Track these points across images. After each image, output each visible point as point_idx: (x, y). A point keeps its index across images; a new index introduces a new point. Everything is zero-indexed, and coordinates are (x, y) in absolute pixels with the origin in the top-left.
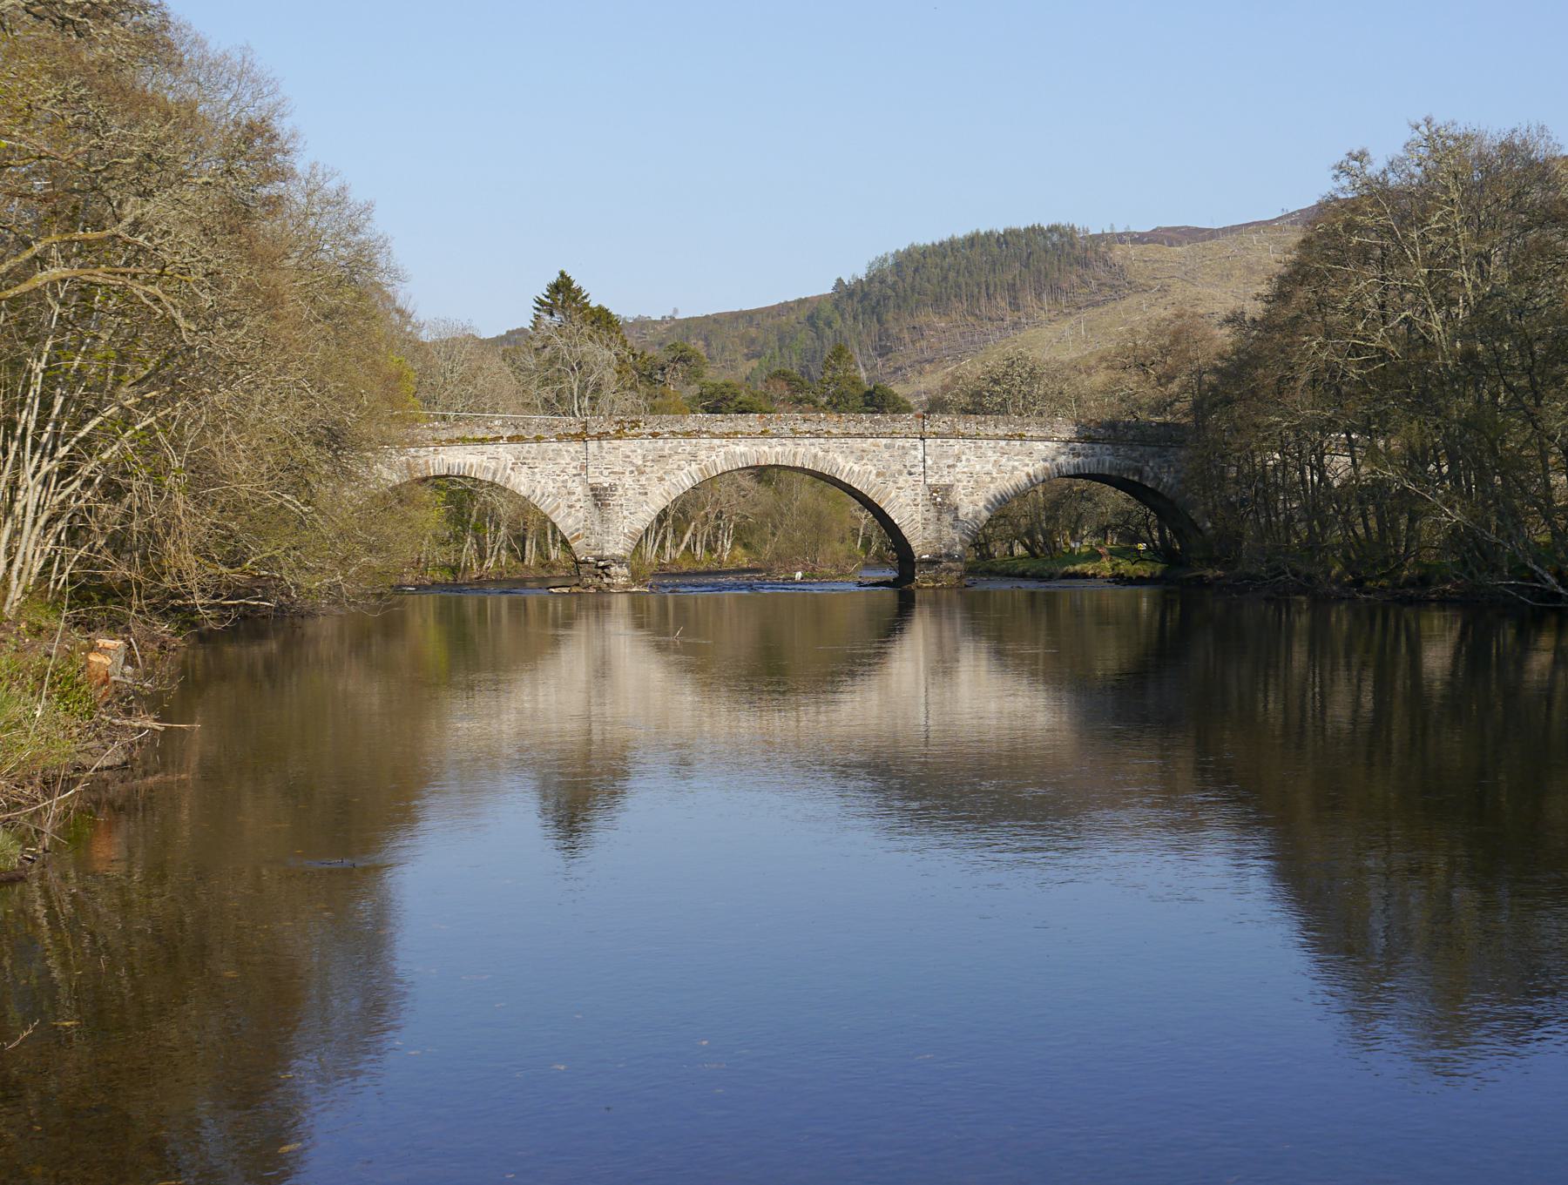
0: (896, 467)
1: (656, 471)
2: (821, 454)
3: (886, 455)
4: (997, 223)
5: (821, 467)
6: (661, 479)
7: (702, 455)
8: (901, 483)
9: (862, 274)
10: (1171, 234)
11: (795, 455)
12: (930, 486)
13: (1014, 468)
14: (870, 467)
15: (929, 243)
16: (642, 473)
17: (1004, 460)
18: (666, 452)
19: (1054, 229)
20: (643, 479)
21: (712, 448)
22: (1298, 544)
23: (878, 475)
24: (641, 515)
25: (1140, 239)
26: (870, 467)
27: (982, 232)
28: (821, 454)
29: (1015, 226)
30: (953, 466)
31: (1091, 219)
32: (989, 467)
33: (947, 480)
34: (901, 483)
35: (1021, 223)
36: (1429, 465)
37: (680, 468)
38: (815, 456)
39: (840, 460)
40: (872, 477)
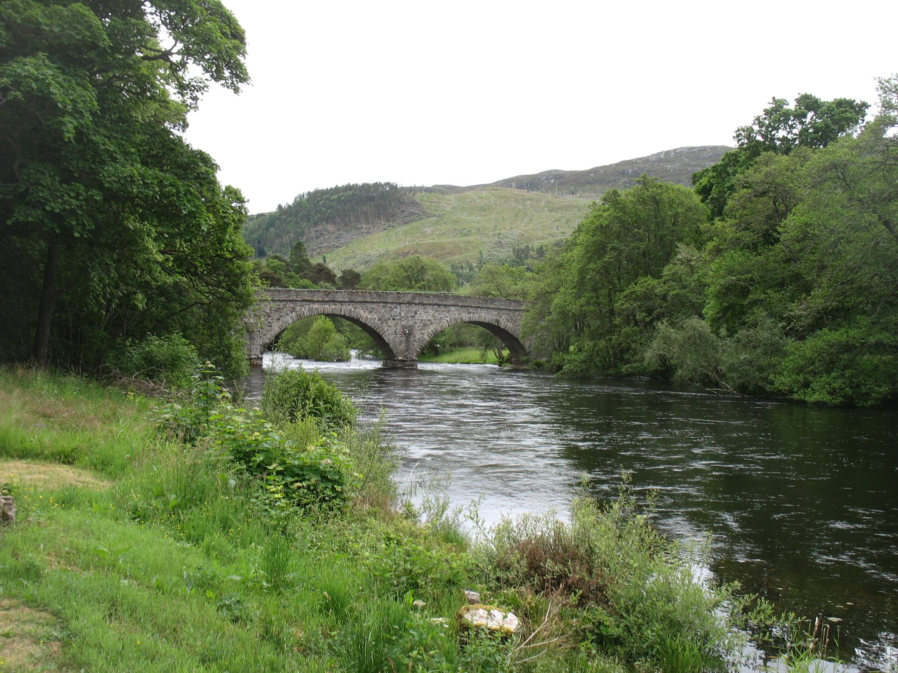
0: (387, 316)
1: (276, 316)
2: (353, 309)
3: (383, 311)
4: (359, 179)
5: (354, 315)
6: (278, 319)
7: (298, 308)
8: (389, 324)
9: (291, 203)
10: (442, 188)
11: (341, 310)
12: (402, 326)
13: (441, 318)
14: (375, 316)
15: (325, 189)
16: (269, 316)
17: (436, 315)
18: (281, 307)
19: (388, 184)
20: (270, 320)
21: (303, 306)
22: (108, 17)
23: (379, 320)
24: (269, 336)
25: (428, 190)
26: (375, 316)
27: (351, 184)
28: (353, 309)
29: (368, 182)
30: (414, 316)
31: (404, 181)
32: (430, 318)
33: (411, 323)
34: (389, 324)
35: (371, 181)
36: (758, 141)
37: (287, 315)
38: (350, 310)
39: (362, 312)
40: (376, 321)
